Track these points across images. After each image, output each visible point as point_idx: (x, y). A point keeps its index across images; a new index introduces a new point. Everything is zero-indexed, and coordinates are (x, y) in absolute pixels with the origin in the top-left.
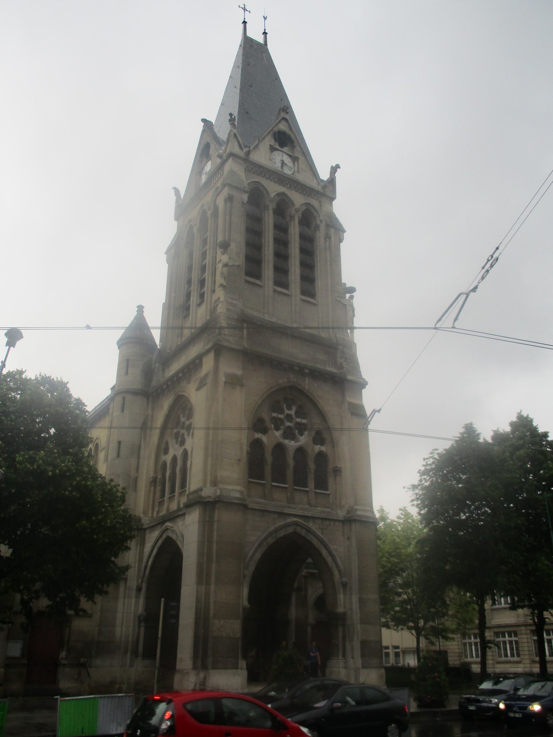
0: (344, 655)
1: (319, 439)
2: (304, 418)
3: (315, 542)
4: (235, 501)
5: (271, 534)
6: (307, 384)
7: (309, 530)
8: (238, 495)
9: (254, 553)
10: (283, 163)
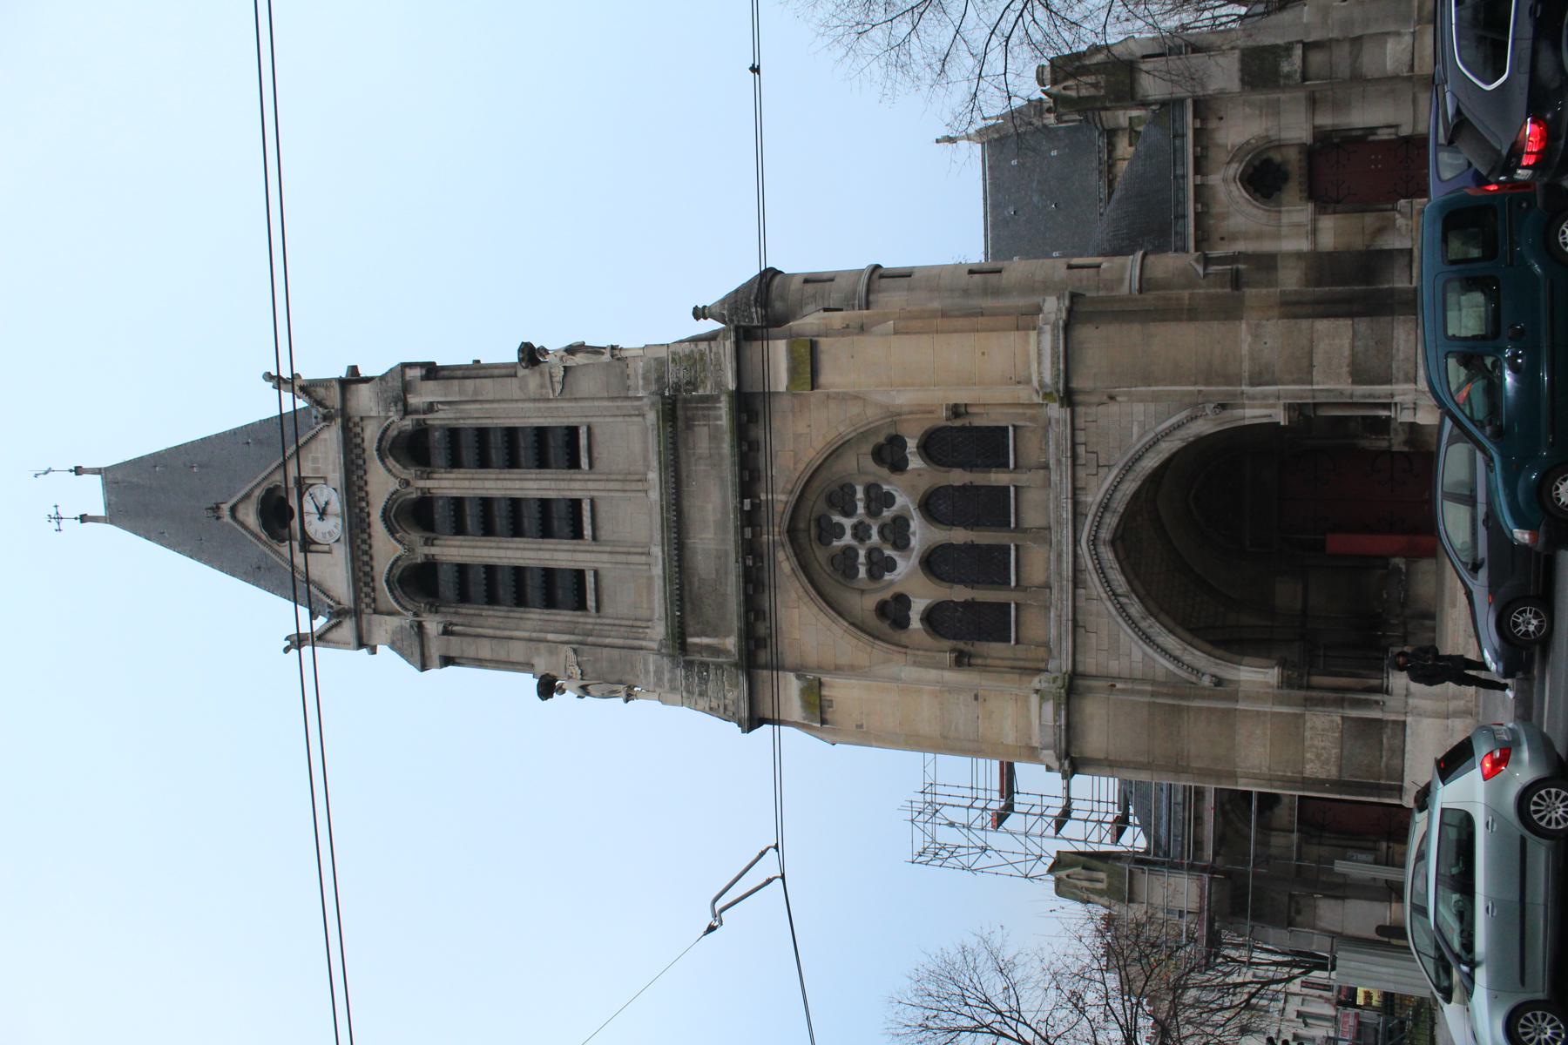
0: (1387, 406)
1: (890, 453)
2: (857, 555)
3: (1130, 487)
4: (1063, 721)
5: (1122, 609)
6: (779, 496)
7: (1105, 507)
8: (1049, 707)
9: (1165, 652)
10: (323, 513)
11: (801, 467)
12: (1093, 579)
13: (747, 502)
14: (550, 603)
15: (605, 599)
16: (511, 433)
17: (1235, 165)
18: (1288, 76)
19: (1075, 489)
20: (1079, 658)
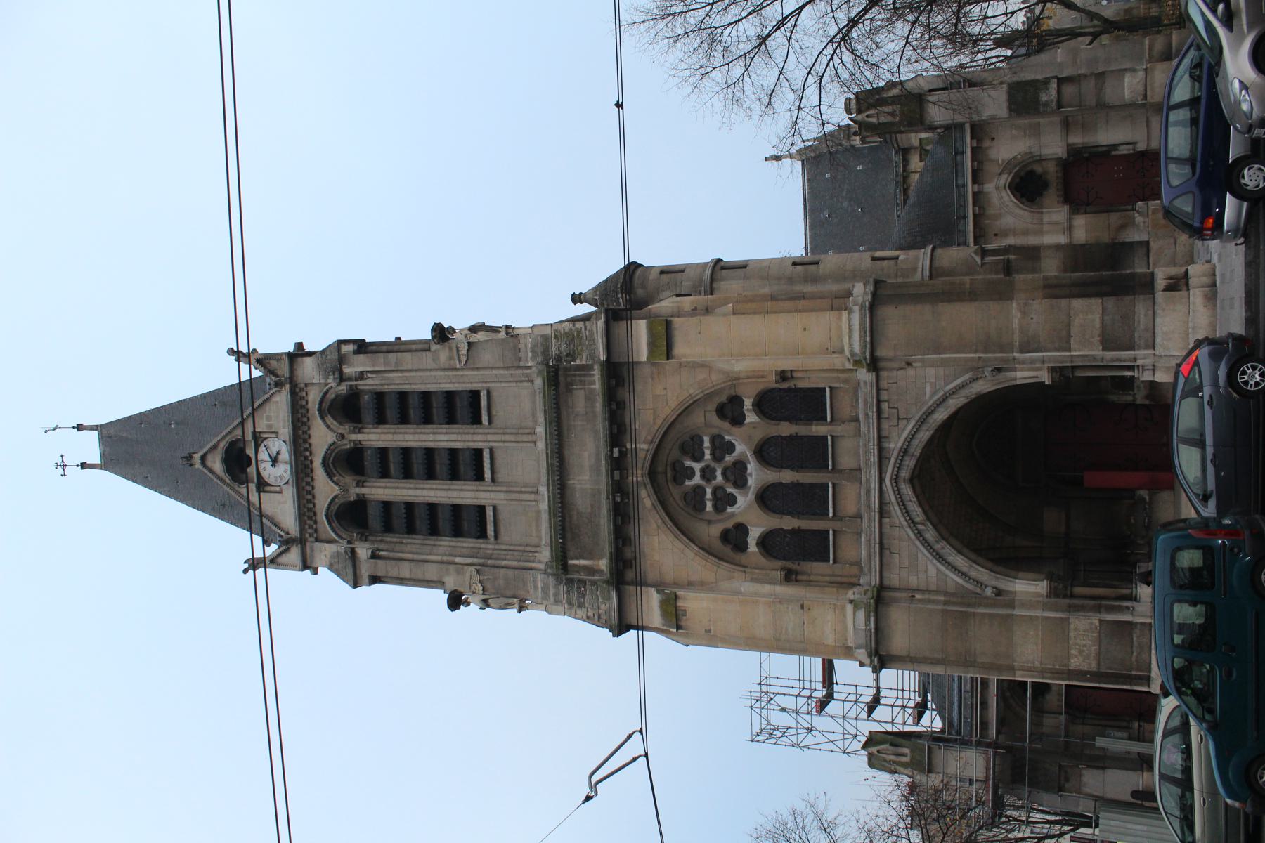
0: (1131, 368)
1: (730, 410)
2: (702, 442)
3: (924, 435)
5: (919, 534)
6: (642, 446)
7: (904, 452)
8: (861, 615)
10: (275, 461)
11: (659, 422)
12: (895, 510)
13: (616, 450)
14: (457, 532)
15: (502, 529)
16: (426, 396)
17: (1005, 176)
18: (1046, 104)
19: (880, 437)
20: (885, 574)
